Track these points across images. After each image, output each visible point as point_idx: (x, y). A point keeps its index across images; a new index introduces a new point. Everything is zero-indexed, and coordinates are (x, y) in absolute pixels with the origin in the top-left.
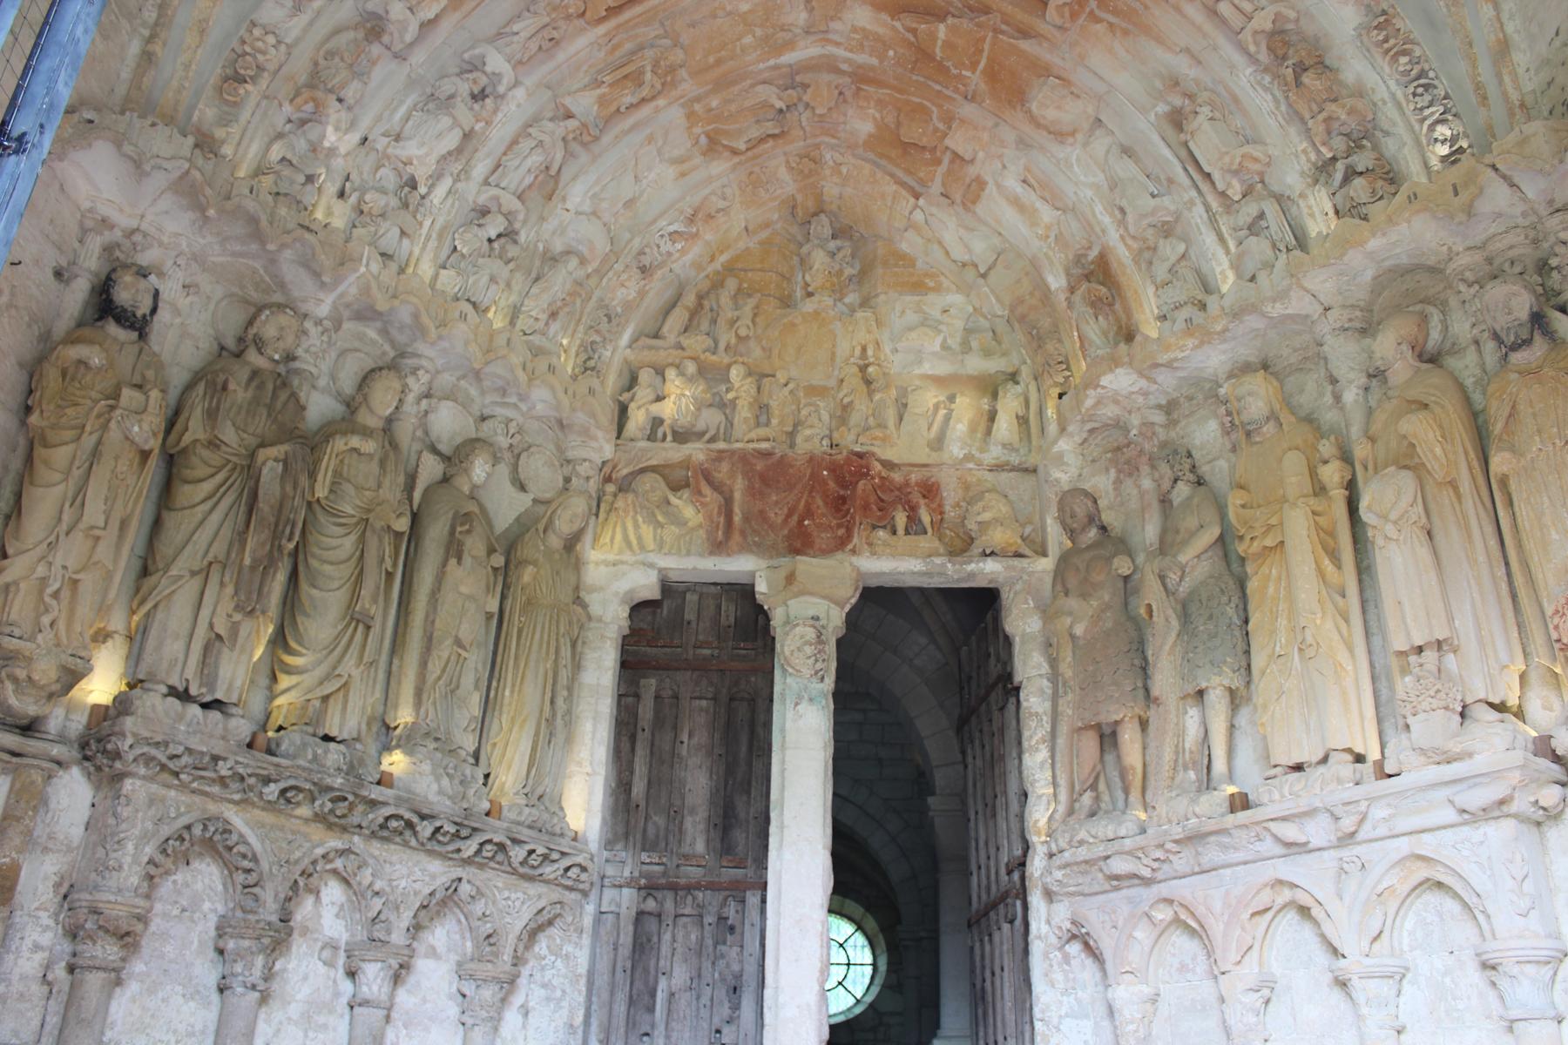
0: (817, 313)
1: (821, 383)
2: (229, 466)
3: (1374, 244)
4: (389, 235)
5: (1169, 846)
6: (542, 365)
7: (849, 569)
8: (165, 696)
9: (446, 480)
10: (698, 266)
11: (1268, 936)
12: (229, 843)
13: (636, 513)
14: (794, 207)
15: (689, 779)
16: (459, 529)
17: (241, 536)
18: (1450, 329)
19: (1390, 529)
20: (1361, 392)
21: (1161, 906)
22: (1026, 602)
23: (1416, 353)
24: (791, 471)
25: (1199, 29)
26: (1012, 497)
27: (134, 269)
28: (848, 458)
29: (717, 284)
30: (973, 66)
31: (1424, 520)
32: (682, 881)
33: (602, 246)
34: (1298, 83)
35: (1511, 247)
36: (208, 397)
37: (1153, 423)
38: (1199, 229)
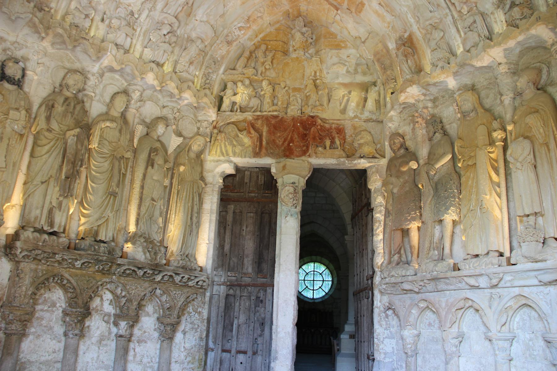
0: (297, 58)
1: (299, 87)
2: (56, 138)
5: (425, 281)
7: (307, 164)
10: (250, 39)
11: (462, 317)
13: (225, 141)
14: (289, 14)
15: (246, 244)
16: (152, 154)
18: (551, 74)
19: (518, 165)
20: (512, 100)
21: (422, 301)
23: (535, 86)
24: (285, 123)
26: (372, 133)
27: (13, 60)
28: (308, 118)
29: (257, 47)
31: (533, 161)
32: (243, 283)
33: (210, 33)
38: (449, 26)
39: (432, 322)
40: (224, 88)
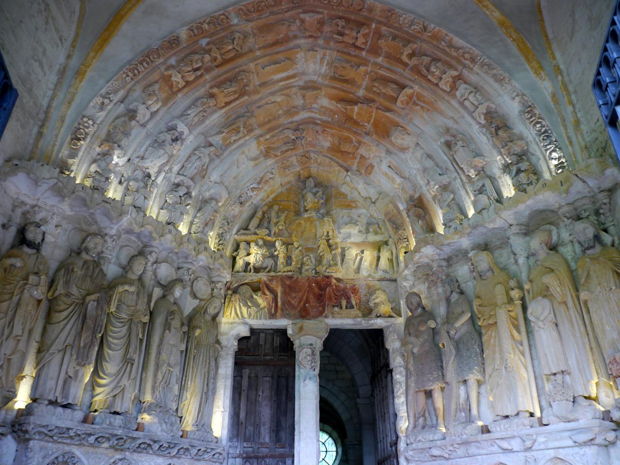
0: (309, 218)
1: (311, 246)
2: (75, 304)
3: (529, 202)
4: (140, 199)
5: (456, 446)
6: (202, 247)
8: (47, 405)
9: (164, 296)
12: (74, 462)
16: (169, 318)
17: (79, 335)
19: (540, 324)
20: (525, 259)
22: (394, 336)
25: (457, 110)
27: (35, 224)
29: (270, 206)
30: (369, 122)
31: (554, 320)
32: (260, 455)
34: (497, 134)
35: (584, 205)
36: (66, 275)
37: (442, 266)
40: (237, 248)
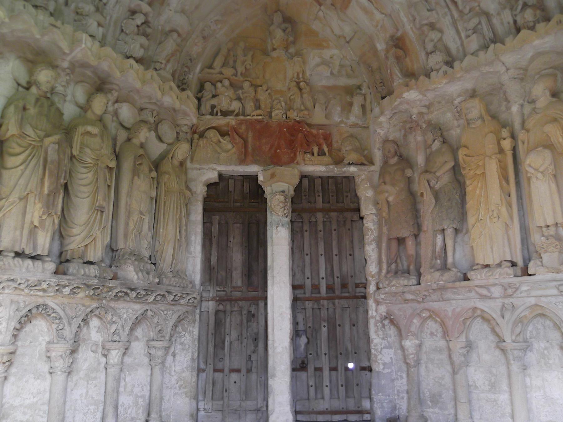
2: (32, 146)
3: (537, 42)
5: (431, 291)
8: (14, 257)
9: (129, 140)
19: (540, 175)
31: (554, 172)
32: (233, 298)
39: (434, 331)
